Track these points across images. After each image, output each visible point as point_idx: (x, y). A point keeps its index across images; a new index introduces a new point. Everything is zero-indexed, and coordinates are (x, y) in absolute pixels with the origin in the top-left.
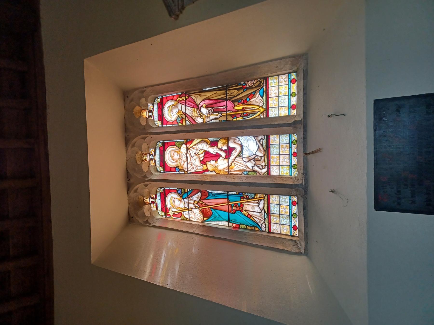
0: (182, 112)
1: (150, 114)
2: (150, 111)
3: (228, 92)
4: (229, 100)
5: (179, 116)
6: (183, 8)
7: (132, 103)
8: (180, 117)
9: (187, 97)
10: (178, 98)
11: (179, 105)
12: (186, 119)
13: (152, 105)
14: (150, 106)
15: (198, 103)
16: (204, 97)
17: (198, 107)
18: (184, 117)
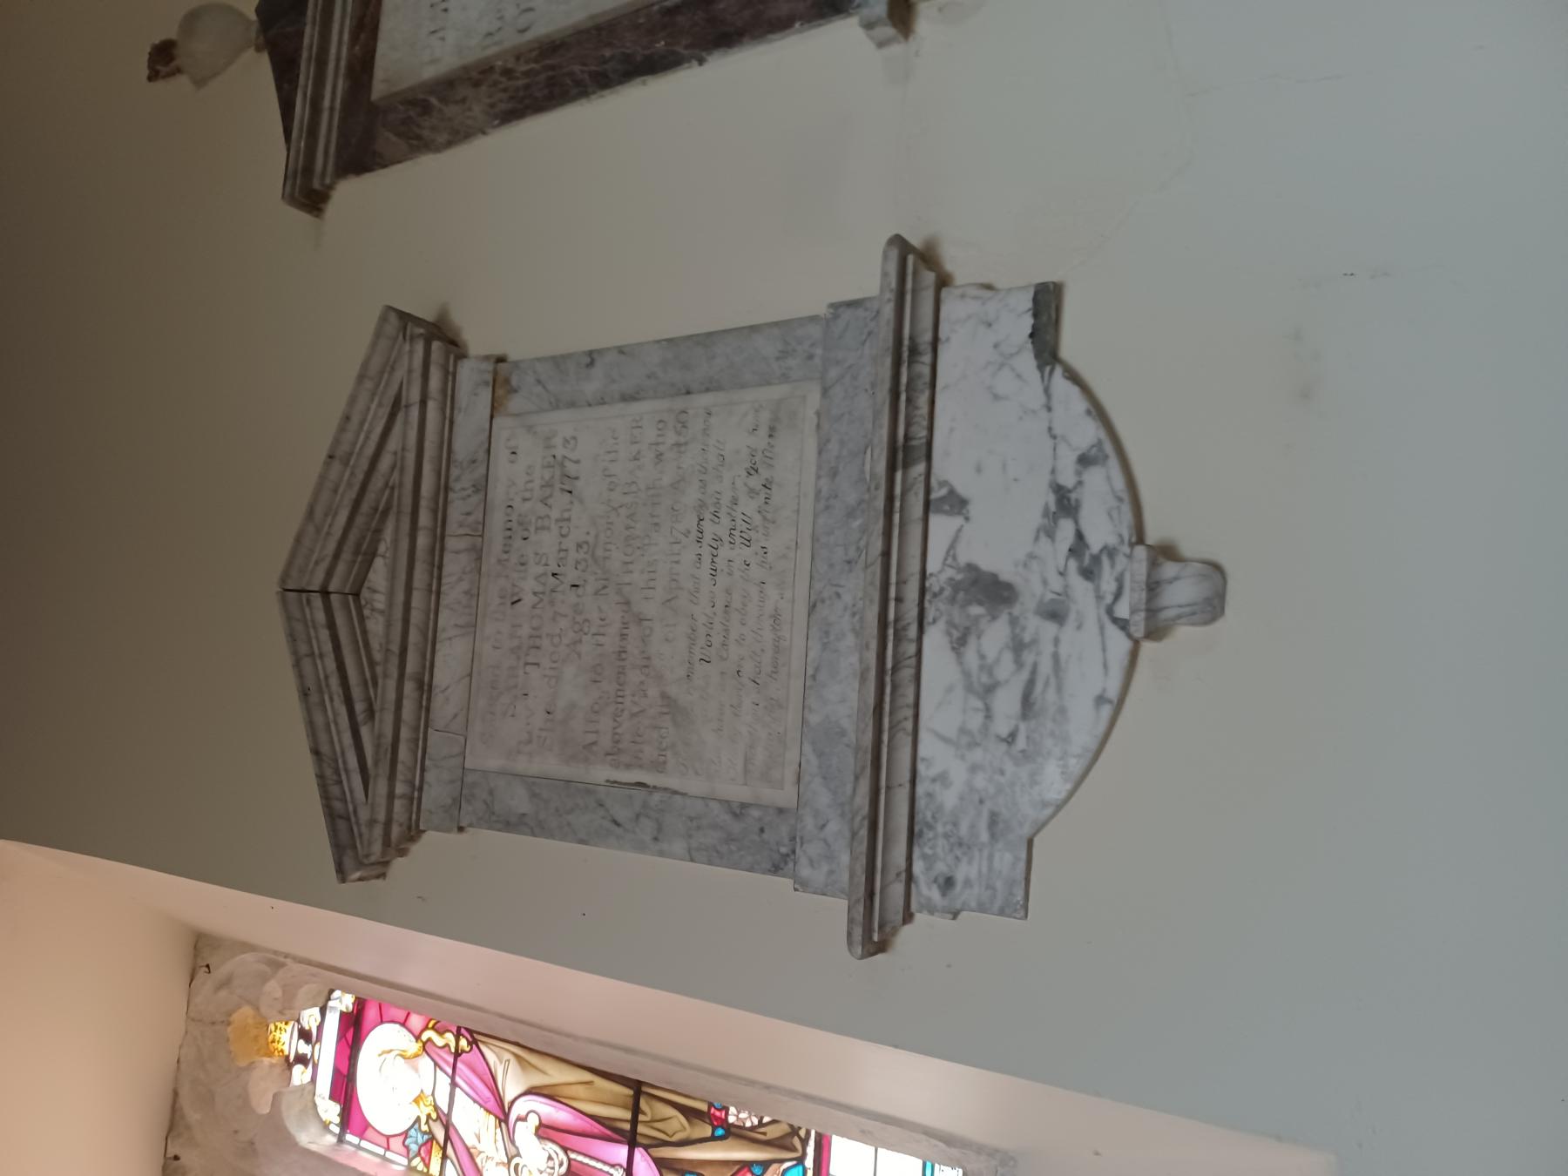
0: (436, 1108)
1: (304, 1048)
2: (305, 1035)
3: (643, 1104)
4: (646, 1148)
5: (418, 1120)
6: (413, 833)
7: (223, 993)
8: (425, 1128)
9: (463, 1043)
10: (426, 1028)
11: (426, 1063)
12: (444, 1149)
13: (316, 1011)
14: (310, 1017)
15: (508, 1099)
16: (537, 1080)
17: (502, 1114)
18: (440, 1134)
